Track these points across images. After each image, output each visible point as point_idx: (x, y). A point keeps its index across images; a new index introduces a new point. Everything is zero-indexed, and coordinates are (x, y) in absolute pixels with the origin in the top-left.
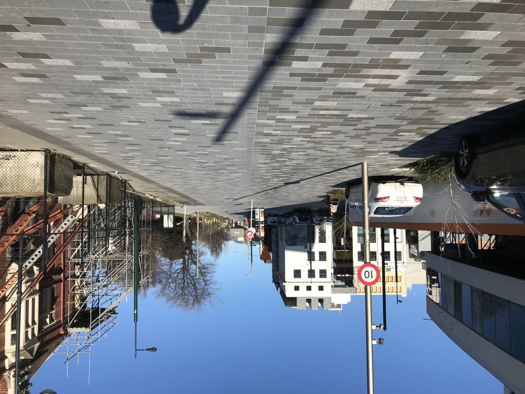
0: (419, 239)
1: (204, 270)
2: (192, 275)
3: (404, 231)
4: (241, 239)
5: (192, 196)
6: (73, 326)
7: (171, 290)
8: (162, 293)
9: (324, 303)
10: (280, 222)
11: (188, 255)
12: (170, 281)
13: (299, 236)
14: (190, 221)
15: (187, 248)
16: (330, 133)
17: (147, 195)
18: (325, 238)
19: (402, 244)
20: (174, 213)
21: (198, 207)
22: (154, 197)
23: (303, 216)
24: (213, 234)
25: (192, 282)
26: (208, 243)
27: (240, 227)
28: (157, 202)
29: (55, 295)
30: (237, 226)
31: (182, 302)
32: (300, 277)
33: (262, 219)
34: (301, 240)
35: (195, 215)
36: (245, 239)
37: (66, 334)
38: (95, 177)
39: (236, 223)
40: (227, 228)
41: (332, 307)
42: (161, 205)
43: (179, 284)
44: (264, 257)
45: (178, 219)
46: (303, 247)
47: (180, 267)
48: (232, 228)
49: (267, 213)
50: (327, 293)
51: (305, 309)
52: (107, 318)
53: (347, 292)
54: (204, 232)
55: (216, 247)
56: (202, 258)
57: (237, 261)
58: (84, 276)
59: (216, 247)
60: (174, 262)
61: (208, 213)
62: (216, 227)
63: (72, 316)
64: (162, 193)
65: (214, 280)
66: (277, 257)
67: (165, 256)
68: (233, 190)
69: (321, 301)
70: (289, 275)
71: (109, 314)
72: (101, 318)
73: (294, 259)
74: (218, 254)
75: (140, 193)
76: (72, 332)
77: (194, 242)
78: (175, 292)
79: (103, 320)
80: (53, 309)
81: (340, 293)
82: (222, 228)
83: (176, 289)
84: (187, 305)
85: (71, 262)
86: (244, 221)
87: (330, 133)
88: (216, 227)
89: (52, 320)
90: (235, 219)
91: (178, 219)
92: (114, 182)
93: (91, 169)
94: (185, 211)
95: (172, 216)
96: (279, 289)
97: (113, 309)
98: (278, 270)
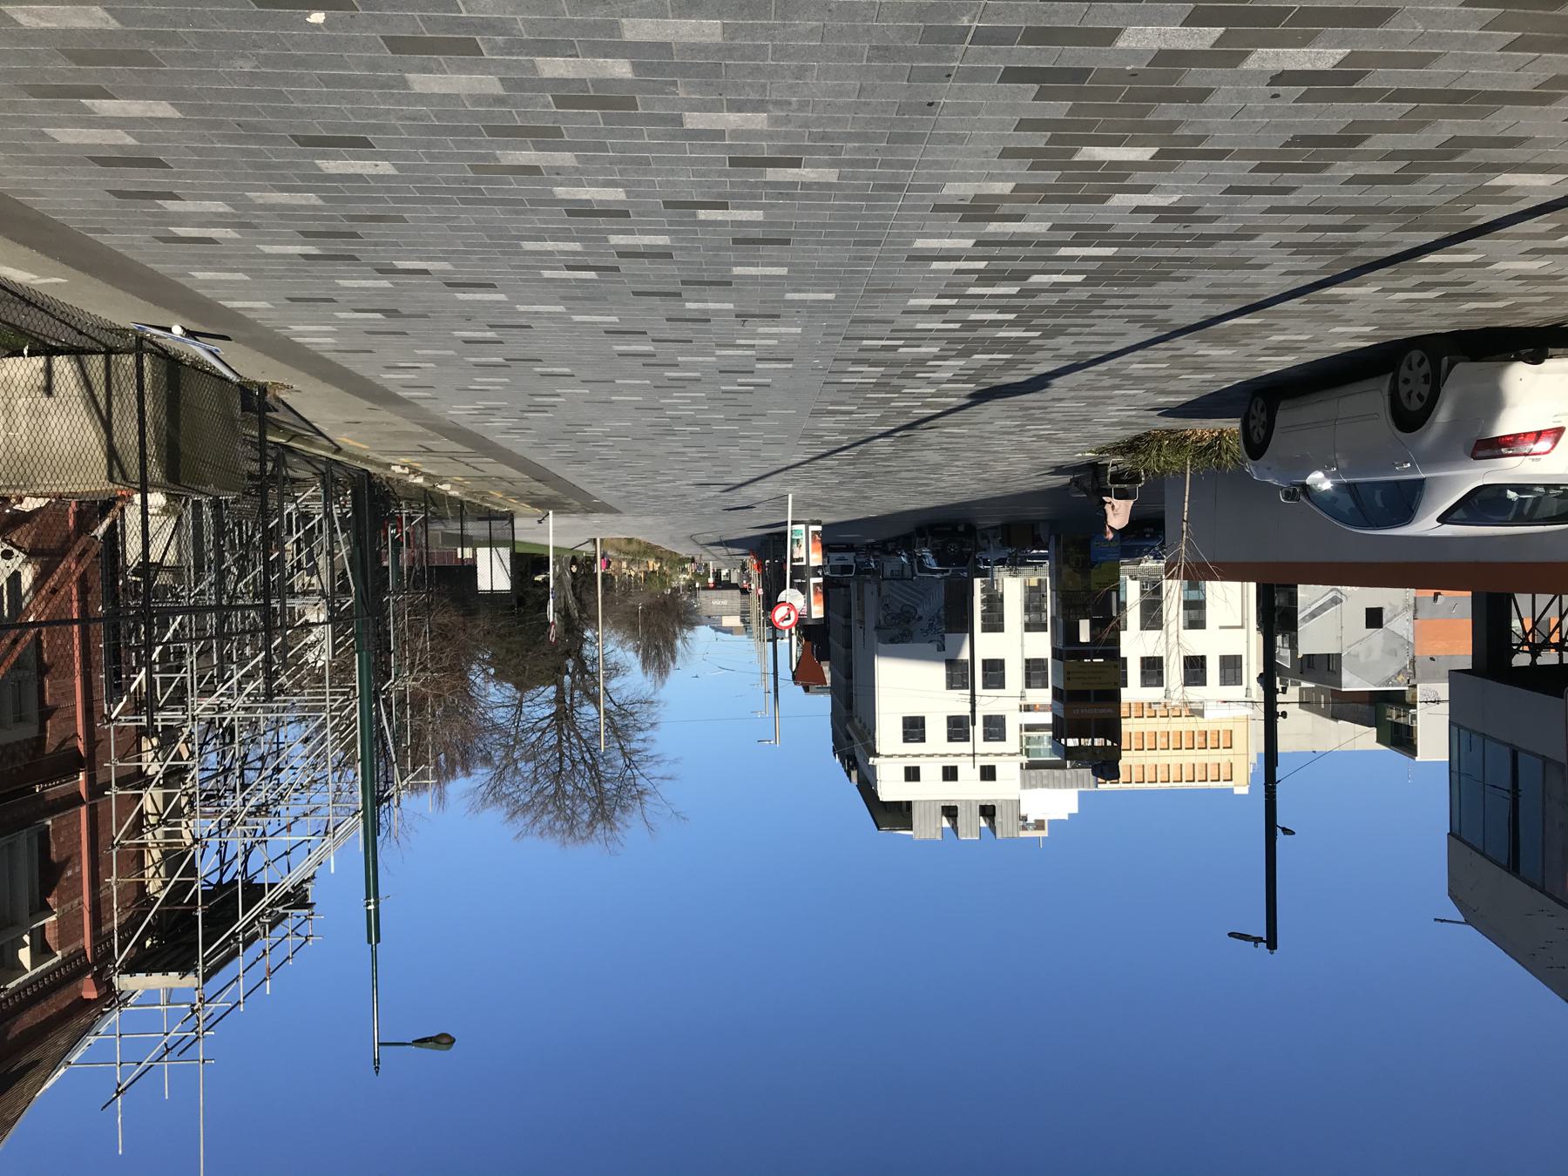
0: (1300, 617)
1: (621, 723)
2: (585, 736)
3: (1253, 586)
4: (734, 621)
5: (569, 473)
6: (131, 968)
7: (518, 788)
8: (494, 794)
9: (998, 819)
10: (862, 570)
11: (572, 676)
12: (516, 755)
13: (920, 612)
14: (574, 569)
15: (568, 654)
16: (957, 326)
17: (397, 469)
18: (1001, 618)
19: (1244, 631)
20: (512, 543)
21: (596, 519)
22: (428, 477)
23: (953, 549)
24: (649, 609)
25: (587, 756)
26: (634, 637)
27: (728, 586)
28: (443, 498)
29: (54, 857)
30: (722, 585)
31: (557, 818)
32: (923, 740)
33: (816, 559)
34: (924, 624)
35: (589, 548)
36: (743, 621)
37: (110, 996)
38: (96, 363)
39: (717, 575)
40: (690, 587)
41: (1024, 828)
42: (462, 510)
43: (546, 764)
44: (805, 676)
45: (527, 564)
46: (933, 647)
47: (548, 712)
48: (707, 588)
49: (831, 540)
50: (1007, 787)
51: (939, 837)
52: (272, 926)
53: (1067, 784)
54: (621, 602)
55: (657, 647)
56: (614, 684)
57: (720, 692)
58: (175, 775)
59: (657, 647)
60: (529, 694)
61: (630, 541)
62: (656, 587)
63: (128, 928)
64: (453, 456)
65: (654, 750)
66: (849, 676)
67: (500, 677)
68: (732, 438)
69: (988, 811)
70: (888, 733)
71: (280, 909)
72: (245, 930)
73: (905, 685)
74: (663, 670)
75: (367, 460)
76: (132, 988)
77: (588, 634)
78: (535, 788)
79: (256, 936)
80: (48, 911)
81: (1046, 786)
82: (676, 590)
83: (536, 780)
84: (571, 827)
85: (120, 731)
86: (744, 568)
87: (957, 326)
88: (656, 587)
89: (41, 951)
90: (718, 561)
91: (527, 564)
92: (200, 395)
93: (29, 303)
94: (551, 533)
95: (505, 552)
96: (854, 774)
97: (298, 887)
98: (850, 719)
